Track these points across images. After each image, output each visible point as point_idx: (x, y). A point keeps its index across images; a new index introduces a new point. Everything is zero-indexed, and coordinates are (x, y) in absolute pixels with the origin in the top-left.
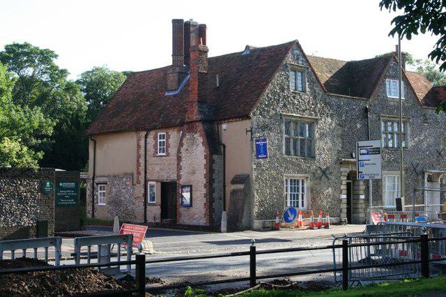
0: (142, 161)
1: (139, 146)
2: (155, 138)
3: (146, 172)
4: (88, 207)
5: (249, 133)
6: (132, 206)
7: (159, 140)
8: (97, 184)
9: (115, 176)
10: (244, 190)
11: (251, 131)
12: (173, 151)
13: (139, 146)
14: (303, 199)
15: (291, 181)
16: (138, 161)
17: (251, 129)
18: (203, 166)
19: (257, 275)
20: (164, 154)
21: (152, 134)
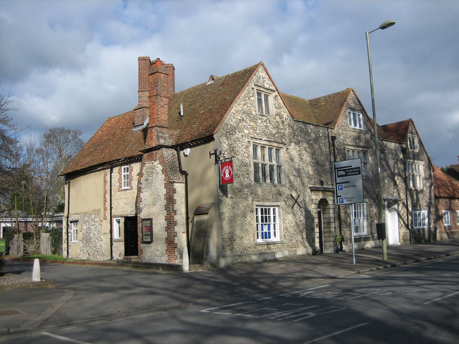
0: (108, 196)
1: (105, 181)
2: (120, 172)
3: (111, 208)
4: (64, 244)
5: (213, 156)
6: (100, 242)
7: (123, 174)
8: (71, 222)
9: (85, 213)
10: (184, 102)
11: (215, 153)
12: (135, 183)
13: (105, 181)
14: (275, 229)
15: (262, 210)
16: (105, 197)
17: (216, 151)
18: (163, 197)
19: (452, 201)
20: (128, 188)
21: (116, 170)
